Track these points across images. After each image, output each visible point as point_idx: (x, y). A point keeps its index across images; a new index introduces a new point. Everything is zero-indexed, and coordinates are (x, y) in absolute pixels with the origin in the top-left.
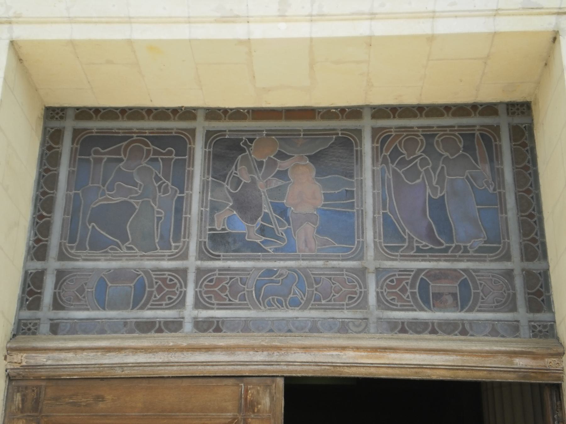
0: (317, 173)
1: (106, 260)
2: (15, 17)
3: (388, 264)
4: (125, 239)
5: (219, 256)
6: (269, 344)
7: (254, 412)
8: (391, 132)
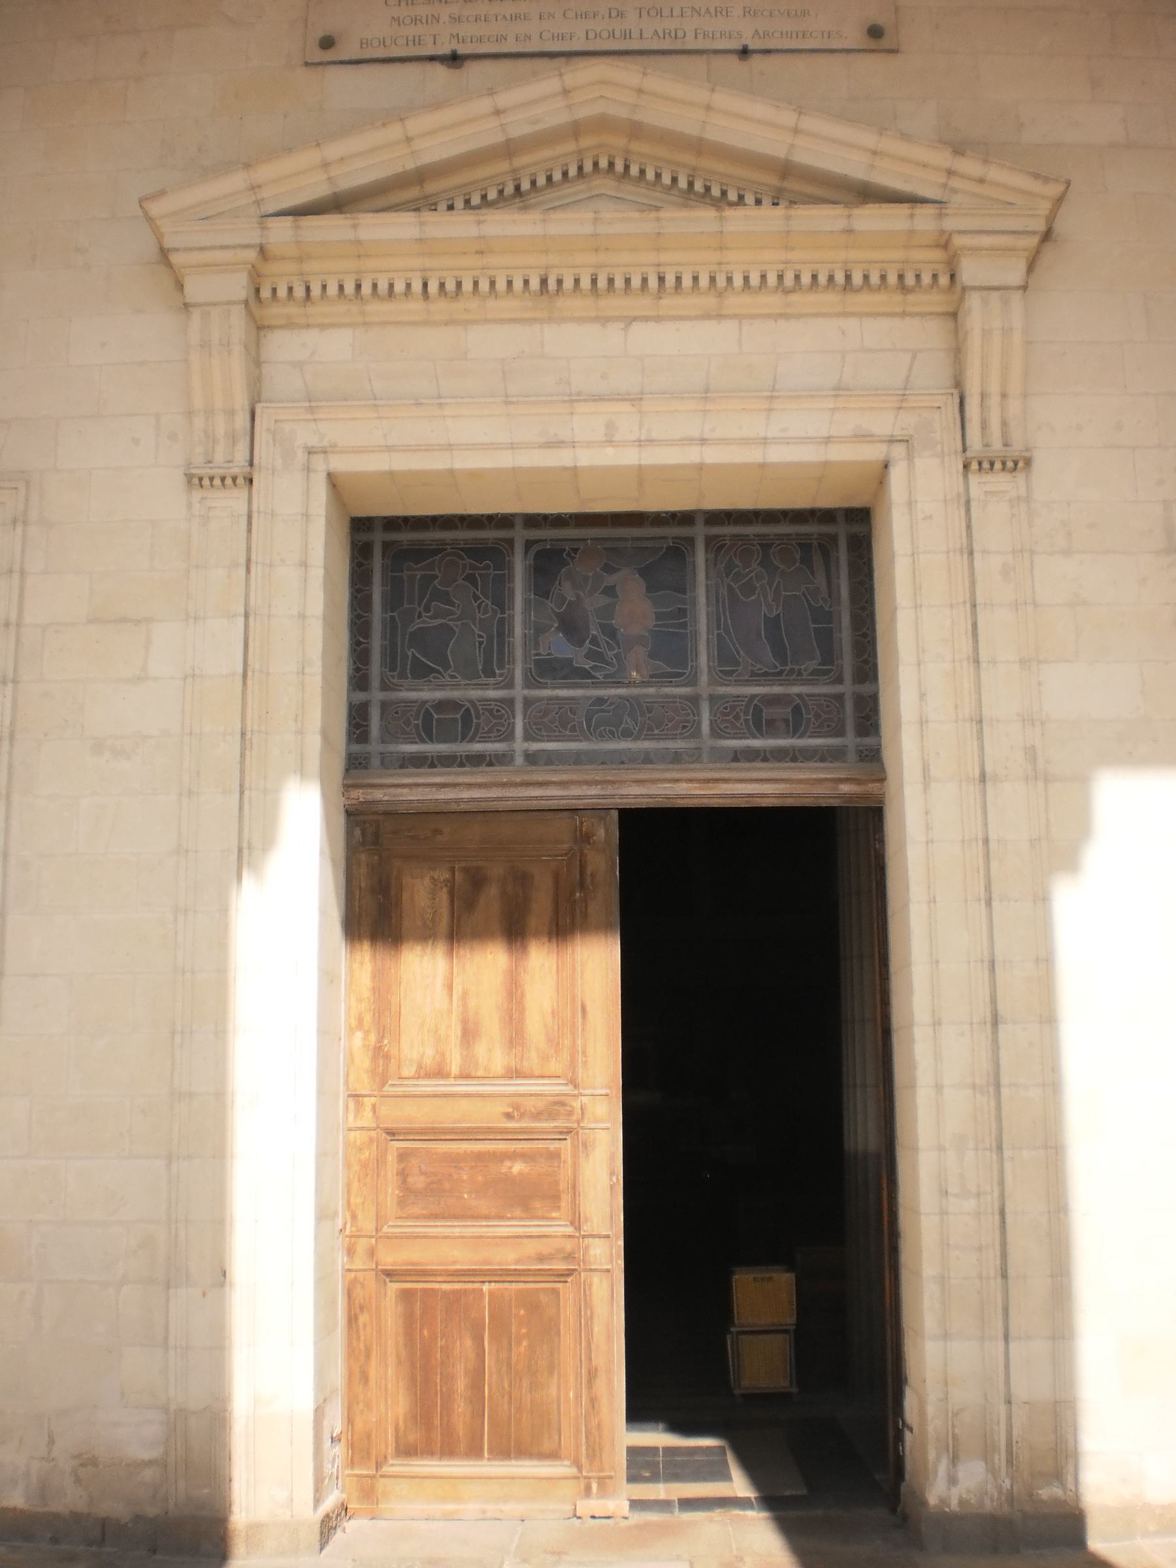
0: (647, 588)
1: (430, 690)
2: (331, 446)
3: (722, 690)
4: (447, 667)
5: (547, 683)
6: (603, 779)
7: (589, 843)
8: (726, 540)
